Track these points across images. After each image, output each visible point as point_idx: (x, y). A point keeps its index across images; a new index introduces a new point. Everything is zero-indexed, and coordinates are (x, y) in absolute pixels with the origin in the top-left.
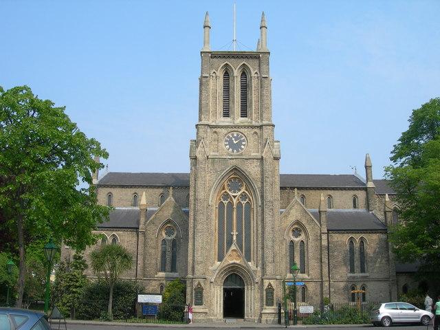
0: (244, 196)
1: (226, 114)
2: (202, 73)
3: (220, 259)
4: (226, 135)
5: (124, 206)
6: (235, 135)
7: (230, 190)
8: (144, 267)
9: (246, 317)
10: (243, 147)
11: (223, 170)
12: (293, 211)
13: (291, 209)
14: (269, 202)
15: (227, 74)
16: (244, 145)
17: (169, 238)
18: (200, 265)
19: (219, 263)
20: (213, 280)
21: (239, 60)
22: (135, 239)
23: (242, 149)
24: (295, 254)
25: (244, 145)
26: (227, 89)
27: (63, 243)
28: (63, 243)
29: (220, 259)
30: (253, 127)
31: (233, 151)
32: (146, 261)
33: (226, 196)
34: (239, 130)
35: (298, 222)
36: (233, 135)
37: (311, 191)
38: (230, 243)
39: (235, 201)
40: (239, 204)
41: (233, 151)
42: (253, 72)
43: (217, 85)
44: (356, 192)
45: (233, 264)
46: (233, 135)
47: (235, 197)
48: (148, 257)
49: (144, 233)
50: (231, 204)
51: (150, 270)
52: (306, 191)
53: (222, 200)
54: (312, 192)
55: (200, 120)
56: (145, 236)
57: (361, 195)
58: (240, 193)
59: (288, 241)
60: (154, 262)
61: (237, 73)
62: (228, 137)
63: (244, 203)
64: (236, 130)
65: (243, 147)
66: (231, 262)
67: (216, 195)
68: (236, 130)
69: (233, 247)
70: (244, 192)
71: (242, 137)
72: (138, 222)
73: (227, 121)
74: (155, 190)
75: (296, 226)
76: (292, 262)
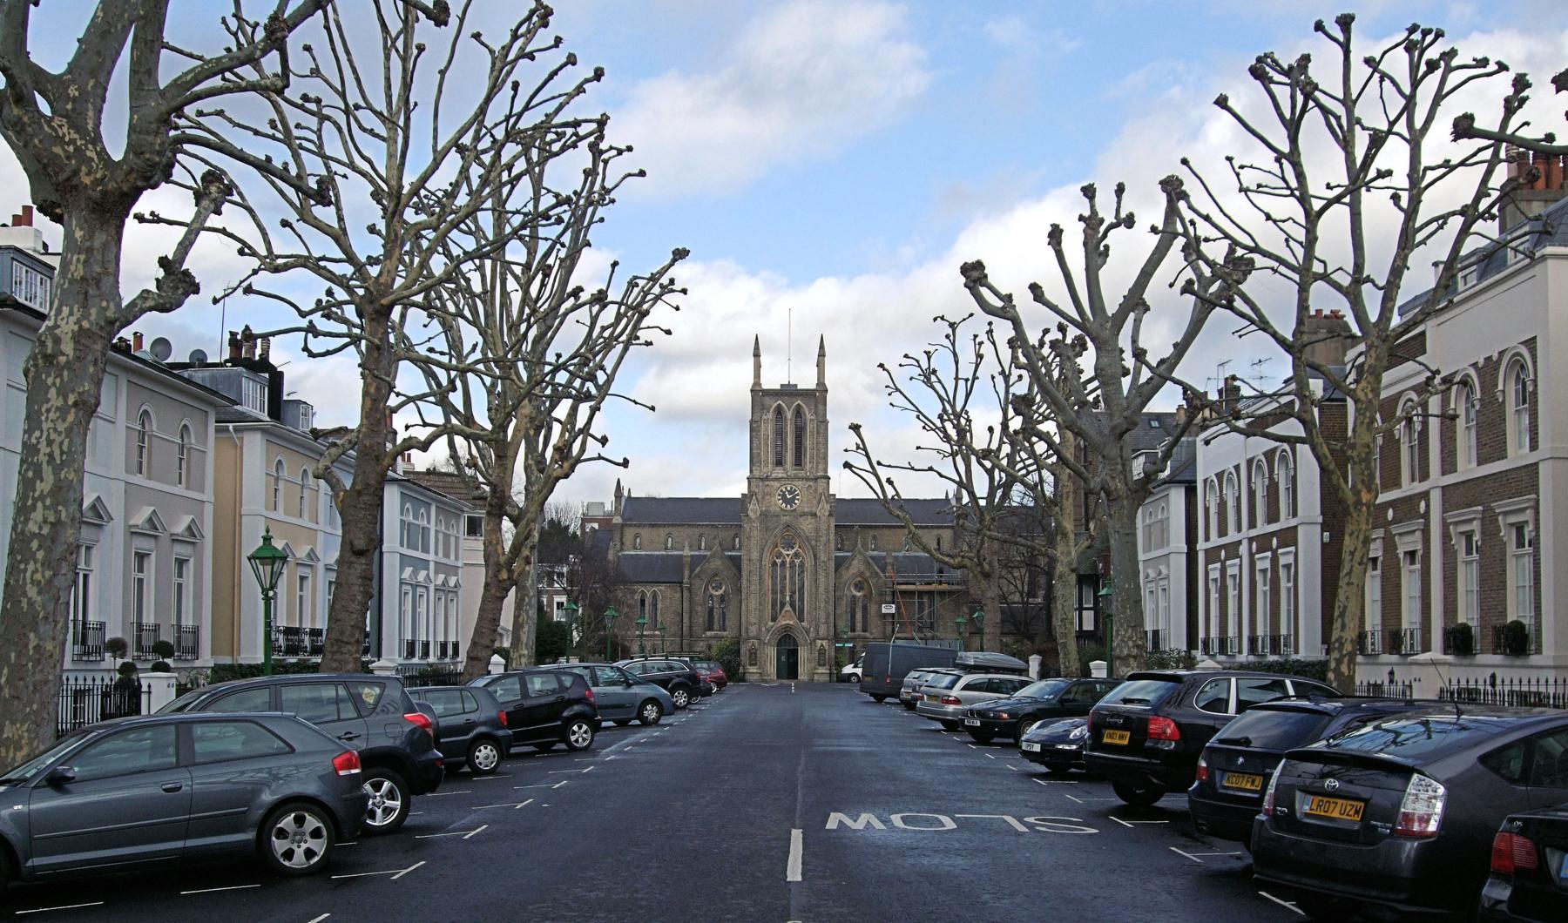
0: (796, 555)
1: (779, 462)
3: (774, 619)
8: (691, 627)
22: (678, 595)
26: (780, 433)
27: (197, 664)
28: (197, 664)
29: (774, 619)
30: (807, 479)
33: (779, 555)
35: (861, 574)
38: (783, 604)
40: (792, 562)
42: (809, 416)
43: (768, 429)
44: (940, 531)
49: (690, 590)
50: (783, 564)
51: (697, 630)
54: (886, 531)
61: (789, 415)
63: (797, 561)
69: (788, 608)
73: (779, 473)
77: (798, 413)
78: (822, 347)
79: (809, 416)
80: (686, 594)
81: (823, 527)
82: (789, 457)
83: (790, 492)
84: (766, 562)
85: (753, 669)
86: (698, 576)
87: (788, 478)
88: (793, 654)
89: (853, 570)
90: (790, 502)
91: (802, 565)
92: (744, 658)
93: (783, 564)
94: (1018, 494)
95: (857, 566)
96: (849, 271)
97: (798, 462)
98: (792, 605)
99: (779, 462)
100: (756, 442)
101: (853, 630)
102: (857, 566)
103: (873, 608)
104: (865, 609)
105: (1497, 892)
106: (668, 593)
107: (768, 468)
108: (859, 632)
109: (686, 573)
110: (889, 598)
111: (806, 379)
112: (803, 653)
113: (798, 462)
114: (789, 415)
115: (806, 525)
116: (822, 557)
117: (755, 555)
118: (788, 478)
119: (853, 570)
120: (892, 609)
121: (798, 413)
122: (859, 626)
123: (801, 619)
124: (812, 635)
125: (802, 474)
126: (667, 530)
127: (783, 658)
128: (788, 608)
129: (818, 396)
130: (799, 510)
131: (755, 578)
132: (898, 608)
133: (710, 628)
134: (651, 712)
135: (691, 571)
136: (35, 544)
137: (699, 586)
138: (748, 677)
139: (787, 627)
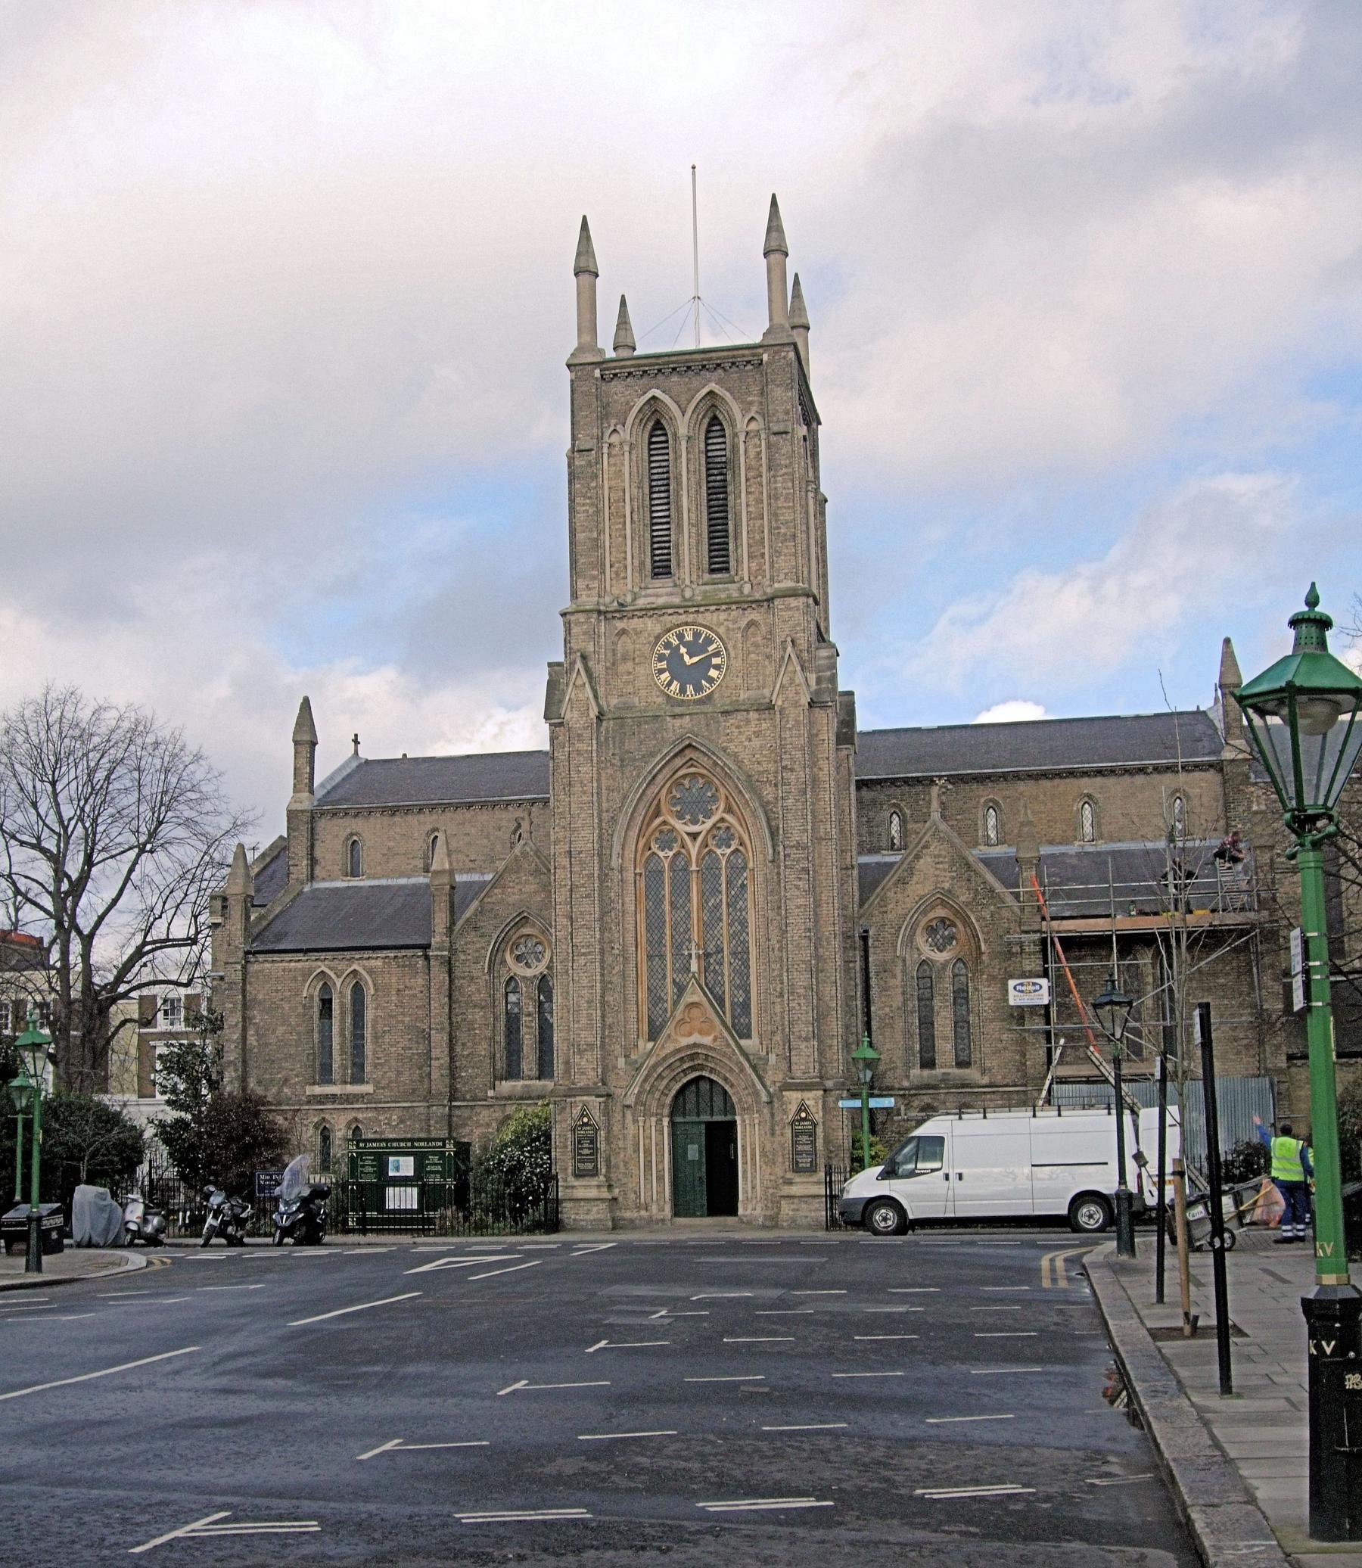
0: (723, 834)
1: (662, 569)
2: (574, 438)
3: (653, 1036)
4: (658, 638)
5: (402, 875)
6: (689, 637)
7: (680, 816)
9: (740, 1211)
10: (713, 673)
11: (653, 755)
12: (925, 864)
13: (918, 857)
14: (798, 846)
15: (657, 426)
16: (717, 667)
17: (529, 973)
18: (588, 1055)
19: (650, 1045)
20: (630, 1100)
21: (696, 382)
23: (711, 680)
24: (937, 1003)
25: (717, 667)
26: (659, 485)
29: (653, 1036)
30: (745, 604)
31: (683, 690)
32: (458, 1049)
33: (668, 837)
34: (700, 619)
35: (944, 898)
36: (680, 636)
37: (1022, 786)
39: (694, 849)
41: (683, 690)
45: (688, 1047)
46: (680, 636)
47: (694, 836)
48: (462, 1036)
50: (680, 871)
51: (475, 1077)
52: (1002, 785)
53: (655, 848)
54: (1024, 787)
55: (574, 595)
56: (450, 972)
57: (1204, 784)
58: (710, 823)
59: (912, 959)
60: (483, 1049)
61: (683, 425)
62: (668, 645)
64: (690, 618)
65: (713, 673)
66: (685, 1041)
67: (633, 834)
68: (690, 618)
69: (694, 995)
70: (722, 820)
71: (712, 642)
72: (430, 932)
73: (661, 592)
74: (498, 813)
75: (940, 912)
76: (1172, 999)
78: (623, 303)
79: (741, 425)
80: (440, 975)
81: (796, 738)
82: (689, 545)
84: (626, 857)
85: (588, 1189)
86: (473, 925)
87: (686, 607)
88: (721, 1140)
89: (920, 887)
90: (696, 675)
91: (737, 869)
92: (562, 1158)
93: (680, 871)
95: (930, 873)
97: (719, 560)
99: (662, 569)
100: (584, 509)
101: (928, 1063)
102: (930, 873)
103: (983, 998)
104: (961, 996)
106: (393, 977)
107: (629, 583)
108: (945, 1066)
109: (441, 920)
110: (1034, 963)
112: (751, 1139)
113: (719, 560)
114: (683, 425)
115: (746, 743)
116: (796, 832)
117: (586, 839)
118: (686, 607)
119: (920, 887)
120: (1041, 993)
122: (945, 1049)
124: (774, 1076)
125: (732, 590)
126: (428, 820)
127: (694, 1152)
128: (694, 995)
130: (721, 702)
131: (589, 909)
132: (1059, 989)
133: (512, 1072)
134: (1217, 1243)
135: (453, 911)
137: (475, 949)
138: (569, 1213)
139: (693, 1054)
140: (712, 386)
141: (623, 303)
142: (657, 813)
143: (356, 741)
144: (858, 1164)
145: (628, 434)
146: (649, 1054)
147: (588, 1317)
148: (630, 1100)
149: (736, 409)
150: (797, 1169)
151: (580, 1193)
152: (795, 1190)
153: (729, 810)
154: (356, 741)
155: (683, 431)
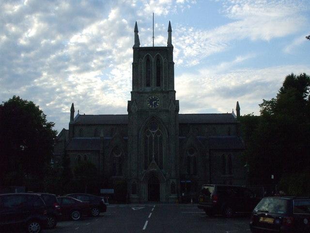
0: (158, 133)
1: (148, 85)
3: (146, 168)
29: (146, 168)
38: (151, 160)
50: (151, 137)
61: (153, 60)
66: (152, 170)
73: (148, 89)
77: (158, 60)
78: (170, 22)
82: (154, 81)
83: (155, 103)
85: (133, 196)
91: (161, 138)
94: (181, 25)
96: (37, 79)
97: (158, 84)
98: (156, 160)
105: (306, 221)
111: (161, 41)
112: (163, 188)
113: (158, 84)
114: (153, 60)
121: (158, 60)
123: (161, 168)
128: (154, 161)
129: (168, 50)
136: (176, 6)
140: (85, 154)
141: (170, 22)
142: (147, 128)
143: (78, 111)
144: (191, 6)
145: (143, 61)
146: (145, 172)
147: (153, 143)
148: (142, 180)
149: (162, 57)
150: (172, 193)
151: (133, 197)
152: (171, 197)
153: (160, 129)
154: (78, 111)
155: (153, 61)
